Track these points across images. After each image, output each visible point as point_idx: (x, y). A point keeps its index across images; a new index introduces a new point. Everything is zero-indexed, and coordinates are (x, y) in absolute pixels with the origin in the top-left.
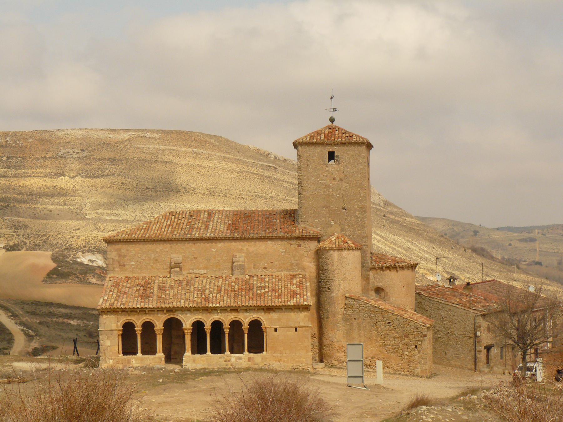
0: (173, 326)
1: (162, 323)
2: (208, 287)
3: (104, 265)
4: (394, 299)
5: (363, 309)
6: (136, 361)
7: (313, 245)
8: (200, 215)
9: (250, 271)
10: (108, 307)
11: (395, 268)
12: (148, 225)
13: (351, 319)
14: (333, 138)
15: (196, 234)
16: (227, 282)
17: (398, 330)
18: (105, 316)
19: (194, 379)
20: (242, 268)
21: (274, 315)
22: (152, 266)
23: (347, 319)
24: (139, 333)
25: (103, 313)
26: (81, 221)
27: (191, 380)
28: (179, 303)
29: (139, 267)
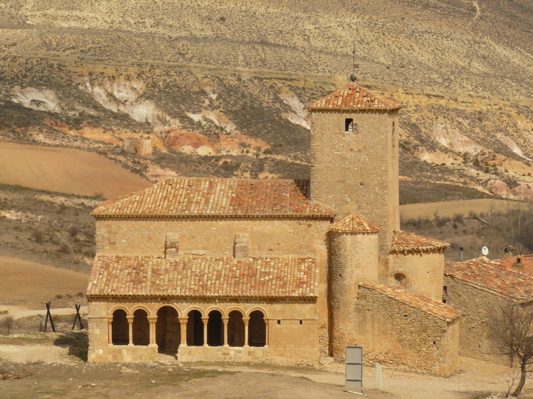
0: (167, 315)
1: (156, 312)
2: (206, 271)
3: (58, 110)
4: (416, 286)
5: (377, 300)
6: (127, 351)
7: (326, 226)
8: (200, 185)
9: (254, 253)
10: (97, 293)
11: (418, 252)
12: (142, 197)
13: (364, 310)
14: (351, 104)
15: (195, 210)
16: (228, 266)
17: (415, 324)
18: (94, 303)
19: (187, 381)
20: (244, 249)
21: (278, 307)
22: (145, 245)
23: (359, 310)
24: (130, 321)
25: (92, 299)
26: (19, 31)
27: (183, 382)
28: (174, 291)
29: (131, 245)
